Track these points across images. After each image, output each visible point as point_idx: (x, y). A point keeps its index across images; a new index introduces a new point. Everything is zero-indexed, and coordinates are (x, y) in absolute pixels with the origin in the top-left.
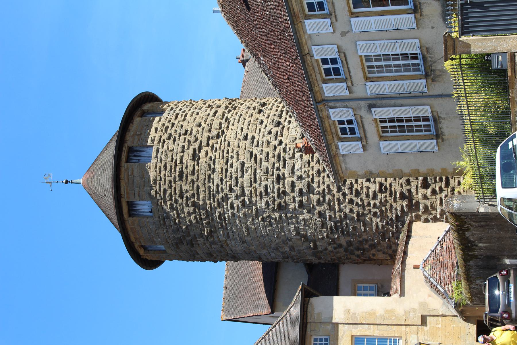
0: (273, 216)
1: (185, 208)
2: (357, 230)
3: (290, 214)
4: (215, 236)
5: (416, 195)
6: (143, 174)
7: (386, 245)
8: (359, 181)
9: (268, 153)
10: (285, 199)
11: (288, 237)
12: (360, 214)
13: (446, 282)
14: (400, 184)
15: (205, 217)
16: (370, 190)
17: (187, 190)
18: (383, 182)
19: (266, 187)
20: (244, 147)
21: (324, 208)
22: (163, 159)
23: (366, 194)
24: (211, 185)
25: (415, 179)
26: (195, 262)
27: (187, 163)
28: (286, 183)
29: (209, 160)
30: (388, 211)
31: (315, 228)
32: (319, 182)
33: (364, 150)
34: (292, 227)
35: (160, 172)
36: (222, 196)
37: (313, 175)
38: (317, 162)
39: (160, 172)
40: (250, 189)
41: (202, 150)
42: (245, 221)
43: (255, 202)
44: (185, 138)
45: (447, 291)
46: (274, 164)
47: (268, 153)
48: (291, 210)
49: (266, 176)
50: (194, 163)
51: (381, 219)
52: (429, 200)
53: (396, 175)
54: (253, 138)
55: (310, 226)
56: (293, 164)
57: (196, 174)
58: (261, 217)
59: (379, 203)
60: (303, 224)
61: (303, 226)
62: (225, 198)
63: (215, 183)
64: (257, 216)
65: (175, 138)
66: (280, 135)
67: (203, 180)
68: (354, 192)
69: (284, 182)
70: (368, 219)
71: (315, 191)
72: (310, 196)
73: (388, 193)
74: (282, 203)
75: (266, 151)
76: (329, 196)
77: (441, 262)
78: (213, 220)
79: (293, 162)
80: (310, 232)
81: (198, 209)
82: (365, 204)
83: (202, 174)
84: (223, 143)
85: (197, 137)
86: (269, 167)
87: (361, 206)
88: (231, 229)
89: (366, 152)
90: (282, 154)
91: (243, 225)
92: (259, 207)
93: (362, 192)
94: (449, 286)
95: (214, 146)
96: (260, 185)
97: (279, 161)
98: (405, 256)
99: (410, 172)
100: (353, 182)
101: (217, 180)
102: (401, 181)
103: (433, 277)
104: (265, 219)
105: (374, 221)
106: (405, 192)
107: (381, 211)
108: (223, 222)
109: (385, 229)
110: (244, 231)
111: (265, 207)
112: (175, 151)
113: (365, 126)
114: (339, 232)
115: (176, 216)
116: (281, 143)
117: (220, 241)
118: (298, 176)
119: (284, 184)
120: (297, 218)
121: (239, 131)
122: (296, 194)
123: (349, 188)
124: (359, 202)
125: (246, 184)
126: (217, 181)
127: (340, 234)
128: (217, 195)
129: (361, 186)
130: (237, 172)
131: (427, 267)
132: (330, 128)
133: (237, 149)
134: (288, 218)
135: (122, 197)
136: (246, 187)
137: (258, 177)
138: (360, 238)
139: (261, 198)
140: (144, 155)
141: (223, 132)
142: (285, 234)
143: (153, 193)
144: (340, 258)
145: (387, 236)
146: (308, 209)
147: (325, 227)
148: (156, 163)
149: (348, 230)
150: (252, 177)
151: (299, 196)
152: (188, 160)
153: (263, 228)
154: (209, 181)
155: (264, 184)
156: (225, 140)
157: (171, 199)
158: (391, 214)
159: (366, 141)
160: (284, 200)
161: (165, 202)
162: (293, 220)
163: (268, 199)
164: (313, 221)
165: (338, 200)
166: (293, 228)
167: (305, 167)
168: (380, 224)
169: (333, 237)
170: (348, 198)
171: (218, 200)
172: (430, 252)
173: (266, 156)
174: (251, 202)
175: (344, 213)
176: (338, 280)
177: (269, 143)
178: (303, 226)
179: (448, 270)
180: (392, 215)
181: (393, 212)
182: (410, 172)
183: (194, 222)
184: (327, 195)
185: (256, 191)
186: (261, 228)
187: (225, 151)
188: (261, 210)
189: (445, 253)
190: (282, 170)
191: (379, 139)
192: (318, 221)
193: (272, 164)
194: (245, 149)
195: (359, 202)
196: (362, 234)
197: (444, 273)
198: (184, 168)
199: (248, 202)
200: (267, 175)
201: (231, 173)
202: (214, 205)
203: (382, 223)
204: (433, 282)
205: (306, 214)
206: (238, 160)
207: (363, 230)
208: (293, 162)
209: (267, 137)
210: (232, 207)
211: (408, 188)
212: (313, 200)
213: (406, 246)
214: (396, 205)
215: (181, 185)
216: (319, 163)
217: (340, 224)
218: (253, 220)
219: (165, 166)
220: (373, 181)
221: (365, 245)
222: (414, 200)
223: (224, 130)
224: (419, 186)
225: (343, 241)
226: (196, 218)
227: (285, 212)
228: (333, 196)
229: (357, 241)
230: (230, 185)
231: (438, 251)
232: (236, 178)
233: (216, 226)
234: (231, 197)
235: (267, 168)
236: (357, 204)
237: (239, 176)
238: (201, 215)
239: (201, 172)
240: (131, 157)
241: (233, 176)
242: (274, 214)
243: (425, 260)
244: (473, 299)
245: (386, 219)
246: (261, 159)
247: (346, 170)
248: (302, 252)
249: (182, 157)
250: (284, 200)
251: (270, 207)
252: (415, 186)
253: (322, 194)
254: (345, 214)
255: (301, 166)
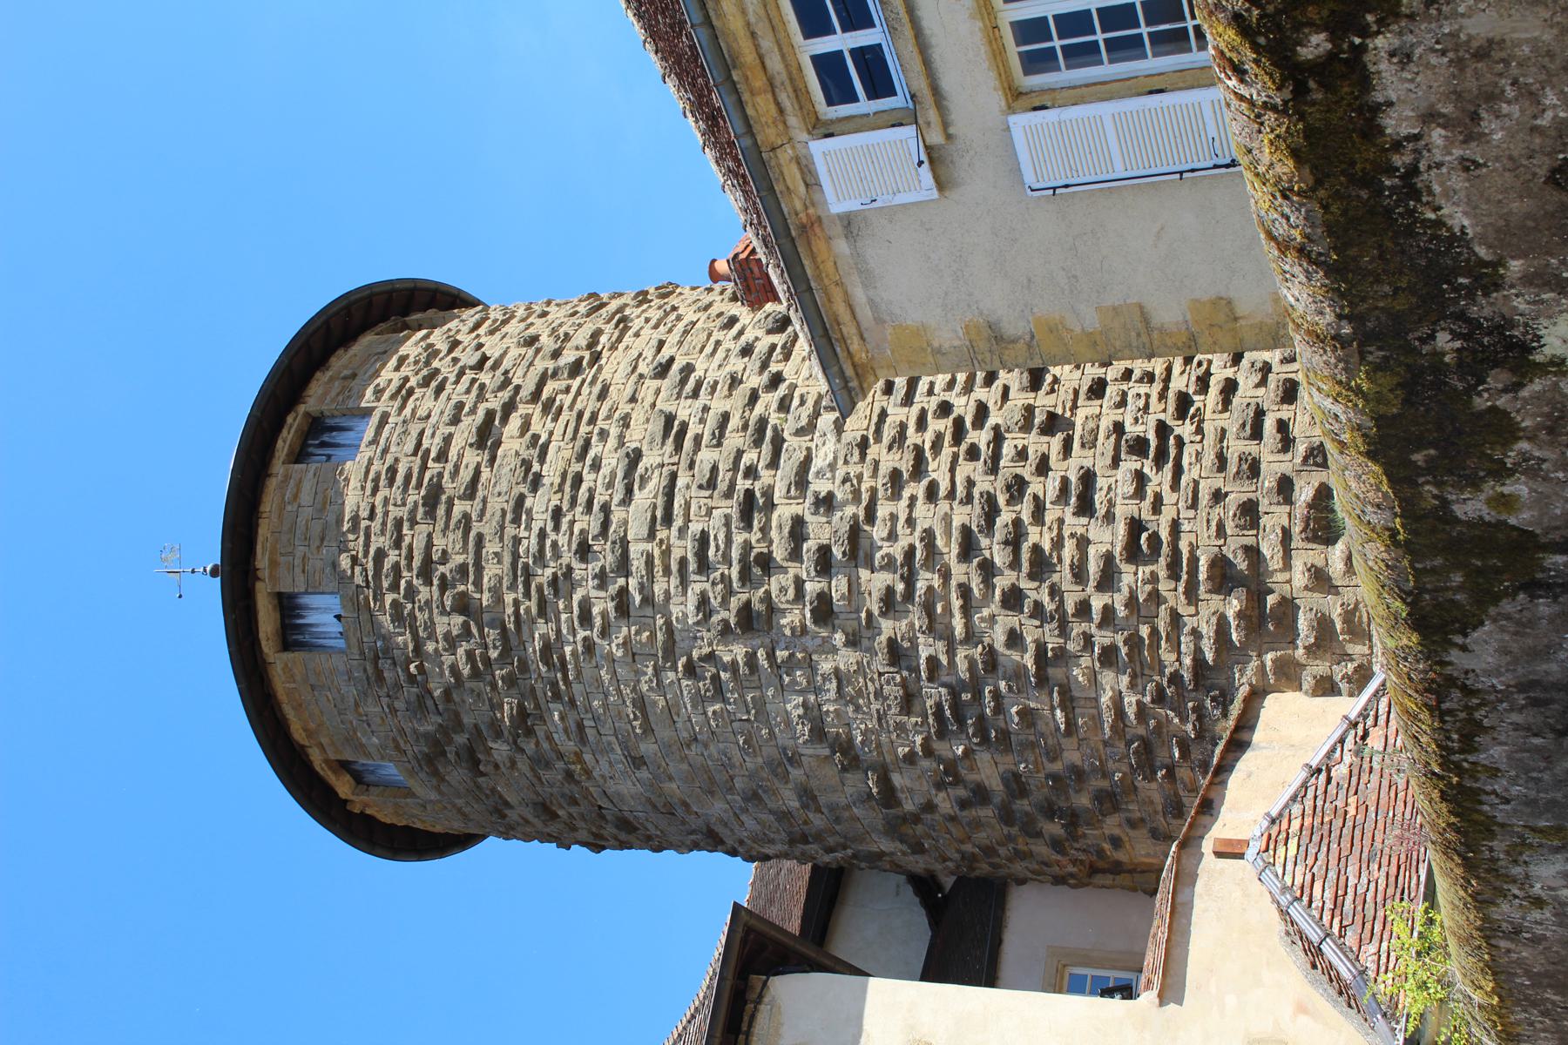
0: (727, 658)
1: (438, 619)
2: (1041, 726)
3: (787, 648)
4: (540, 731)
5: (1281, 570)
6: (325, 497)
7: (1158, 798)
8: (1047, 513)
9: (725, 417)
10: (766, 587)
11: (785, 749)
12: (1050, 654)
13: (1368, 926)
14: (1214, 524)
15: (500, 655)
16: (1092, 550)
17: (444, 552)
18: (1146, 515)
19: (703, 540)
20: (650, 399)
21: (912, 625)
22: (393, 449)
23: (1072, 565)
24: (523, 534)
25: (1279, 503)
26: (515, 843)
27: (461, 456)
28: (774, 524)
29: (528, 448)
30: (1163, 643)
31: (878, 711)
32: (894, 518)
33: (941, 185)
34: (794, 706)
35: (375, 490)
36: (555, 575)
37: (873, 491)
38: (894, 441)
39: (375, 490)
40: (648, 546)
41: (514, 414)
42: (632, 675)
43: (662, 598)
44: (474, 381)
45: (1372, 974)
46: (739, 454)
47: (725, 417)
48: (788, 632)
49: (706, 501)
50: (479, 459)
51: (1133, 677)
52: (1337, 593)
53: (1118, 344)
54: (688, 369)
55: (861, 701)
56: (805, 453)
57: (480, 494)
58: (684, 659)
59: (1126, 606)
60: (832, 695)
61: (835, 701)
62: (563, 582)
63: (536, 526)
64: (670, 651)
65: (445, 379)
66: (780, 357)
67: (499, 513)
68: (1025, 555)
69: (769, 520)
70: (1080, 679)
71: (878, 555)
72: (859, 578)
73: (1162, 561)
74: (757, 606)
75: (720, 411)
76: (928, 575)
77: (1349, 824)
78: (524, 666)
79: (809, 444)
80: (863, 726)
81: (477, 624)
82: (1070, 608)
83: (499, 494)
84: (585, 390)
85: (510, 375)
86: (721, 467)
87: (1052, 618)
88: (588, 709)
89: (953, 195)
90: (774, 419)
91: (626, 691)
92: (677, 618)
93: (1060, 560)
94: (1384, 945)
95: (554, 400)
96: (682, 531)
97: (758, 443)
98: (1205, 819)
99: (1189, 317)
100: (1026, 517)
101: (544, 517)
102: (1218, 510)
103: (1305, 899)
104: (698, 670)
105: (1108, 688)
106: (1235, 557)
107: (1134, 642)
108: (559, 675)
109: (1152, 723)
110: (632, 716)
111: (695, 620)
112: (433, 420)
113: (919, 13)
114: (971, 731)
115: (411, 647)
116: (777, 380)
117: (561, 756)
118: (817, 498)
119: (765, 530)
120: (812, 667)
121: (649, 353)
122: (806, 569)
123: (1006, 543)
124: (1046, 599)
125: (637, 530)
126: (541, 518)
127: (975, 740)
128: (540, 572)
129: (1055, 532)
130: (610, 485)
131: (1281, 851)
132: (757, 47)
133: (627, 408)
134: (779, 667)
135: (259, 579)
136: (638, 540)
137: (678, 501)
138: (1053, 760)
139: (684, 583)
140: (348, 442)
141: (596, 357)
142: (771, 733)
143: (345, 562)
144: (989, 851)
145: (1161, 756)
146: (850, 630)
147: (917, 708)
148: (370, 462)
149: (1002, 725)
150: (660, 501)
151: (819, 573)
152: (464, 448)
153: (694, 706)
154: (516, 521)
155: (695, 527)
156: (593, 382)
157: (395, 587)
158: (1173, 657)
159: (945, 125)
160: (763, 590)
161: (379, 596)
162: (798, 673)
163: (708, 586)
164: (872, 680)
165: (965, 591)
166: (801, 711)
167: (846, 462)
168: (1130, 701)
169: (950, 755)
170: (1002, 583)
171: (540, 589)
172: (1304, 775)
173: (715, 425)
174: (648, 600)
175: (984, 648)
176: (997, 943)
177: (735, 381)
178: (835, 701)
179: (1385, 861)
180: (1178, 660)
181: (1183, 646)
182: (1189, 317)
183: (466, 671)
184: (921, 572)
185: (666, 554)
186: (689, 706)
187: (587, 416)
188: (682, 630)
189: (1375, 777)
190: (766, 476)
191: (1003, 103)
192: (888, 683)
193: (732, 456)
194: (654, 405)
195: (1046, 599)
196: (1060, 744)
197: (1364, 880)
198: (446, 475)
199: (638, 599)
200: (711, 497)
201: (591, 492)
202: (528, 610)
203: (1140, 696)
204: (1336, 961)
205: (843, 651)
206: (621, 443)
207: (1063, 727)
208: (809, 444)
209: (737, 364)
210: (586, 618)
211: (1250, 541)
212: (870, 594)
213: (1217, 780)
214: (1197, 613)
215: (430, 536)
216: (901, 446)
217: (973, 696)
218: (657, 672)
219: (392, 471)
220: (1103, 512)
221: (1078, 792)
222: (1271, 591)
223: (601, 353)
224: (1296, 529)
225: (989, 770)
226: (470, 655)
227: (768, 640)
228: (946, 575)
229: (1042, 775)
230: (582, 531)
231: (1339, 772)
232: (606, 509)
233: (539, 694)
234: (582, 578)
235: (714, 469)
236: (1038, 610)
237: (617, 498)
238: (486, 647)
239: (497, 489)
240: (311, 450)
241: (596, 501)
242: (731, 648)
243: (1274, 814)
244: (1518, 1023)
245: (1157, 678)
246: (698, 439)
247: (879, 321)
248: (847, 814)
249: (448, 440)
250: (763, 590)
251: (715, 619)
252: (1279, 531)
253: (902, 566)
254: (991, 653)
255: (835, 458)
